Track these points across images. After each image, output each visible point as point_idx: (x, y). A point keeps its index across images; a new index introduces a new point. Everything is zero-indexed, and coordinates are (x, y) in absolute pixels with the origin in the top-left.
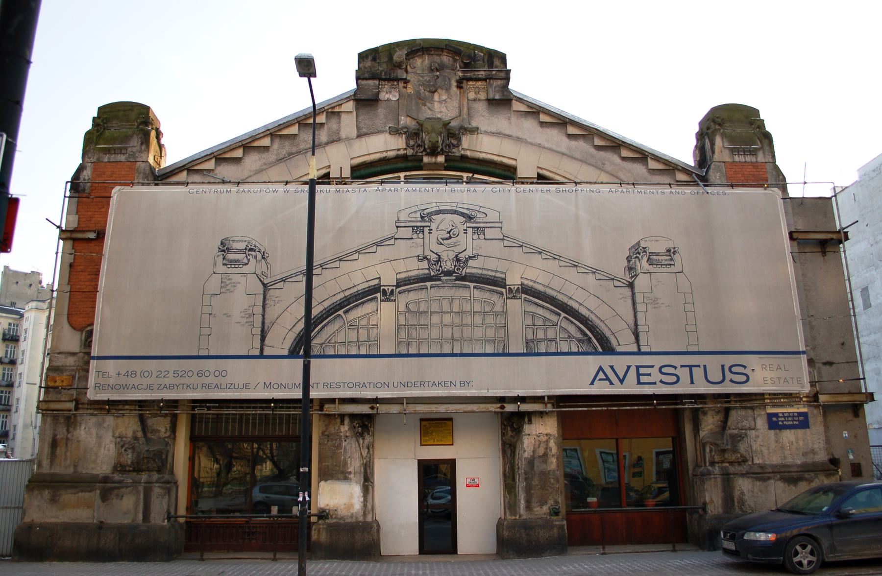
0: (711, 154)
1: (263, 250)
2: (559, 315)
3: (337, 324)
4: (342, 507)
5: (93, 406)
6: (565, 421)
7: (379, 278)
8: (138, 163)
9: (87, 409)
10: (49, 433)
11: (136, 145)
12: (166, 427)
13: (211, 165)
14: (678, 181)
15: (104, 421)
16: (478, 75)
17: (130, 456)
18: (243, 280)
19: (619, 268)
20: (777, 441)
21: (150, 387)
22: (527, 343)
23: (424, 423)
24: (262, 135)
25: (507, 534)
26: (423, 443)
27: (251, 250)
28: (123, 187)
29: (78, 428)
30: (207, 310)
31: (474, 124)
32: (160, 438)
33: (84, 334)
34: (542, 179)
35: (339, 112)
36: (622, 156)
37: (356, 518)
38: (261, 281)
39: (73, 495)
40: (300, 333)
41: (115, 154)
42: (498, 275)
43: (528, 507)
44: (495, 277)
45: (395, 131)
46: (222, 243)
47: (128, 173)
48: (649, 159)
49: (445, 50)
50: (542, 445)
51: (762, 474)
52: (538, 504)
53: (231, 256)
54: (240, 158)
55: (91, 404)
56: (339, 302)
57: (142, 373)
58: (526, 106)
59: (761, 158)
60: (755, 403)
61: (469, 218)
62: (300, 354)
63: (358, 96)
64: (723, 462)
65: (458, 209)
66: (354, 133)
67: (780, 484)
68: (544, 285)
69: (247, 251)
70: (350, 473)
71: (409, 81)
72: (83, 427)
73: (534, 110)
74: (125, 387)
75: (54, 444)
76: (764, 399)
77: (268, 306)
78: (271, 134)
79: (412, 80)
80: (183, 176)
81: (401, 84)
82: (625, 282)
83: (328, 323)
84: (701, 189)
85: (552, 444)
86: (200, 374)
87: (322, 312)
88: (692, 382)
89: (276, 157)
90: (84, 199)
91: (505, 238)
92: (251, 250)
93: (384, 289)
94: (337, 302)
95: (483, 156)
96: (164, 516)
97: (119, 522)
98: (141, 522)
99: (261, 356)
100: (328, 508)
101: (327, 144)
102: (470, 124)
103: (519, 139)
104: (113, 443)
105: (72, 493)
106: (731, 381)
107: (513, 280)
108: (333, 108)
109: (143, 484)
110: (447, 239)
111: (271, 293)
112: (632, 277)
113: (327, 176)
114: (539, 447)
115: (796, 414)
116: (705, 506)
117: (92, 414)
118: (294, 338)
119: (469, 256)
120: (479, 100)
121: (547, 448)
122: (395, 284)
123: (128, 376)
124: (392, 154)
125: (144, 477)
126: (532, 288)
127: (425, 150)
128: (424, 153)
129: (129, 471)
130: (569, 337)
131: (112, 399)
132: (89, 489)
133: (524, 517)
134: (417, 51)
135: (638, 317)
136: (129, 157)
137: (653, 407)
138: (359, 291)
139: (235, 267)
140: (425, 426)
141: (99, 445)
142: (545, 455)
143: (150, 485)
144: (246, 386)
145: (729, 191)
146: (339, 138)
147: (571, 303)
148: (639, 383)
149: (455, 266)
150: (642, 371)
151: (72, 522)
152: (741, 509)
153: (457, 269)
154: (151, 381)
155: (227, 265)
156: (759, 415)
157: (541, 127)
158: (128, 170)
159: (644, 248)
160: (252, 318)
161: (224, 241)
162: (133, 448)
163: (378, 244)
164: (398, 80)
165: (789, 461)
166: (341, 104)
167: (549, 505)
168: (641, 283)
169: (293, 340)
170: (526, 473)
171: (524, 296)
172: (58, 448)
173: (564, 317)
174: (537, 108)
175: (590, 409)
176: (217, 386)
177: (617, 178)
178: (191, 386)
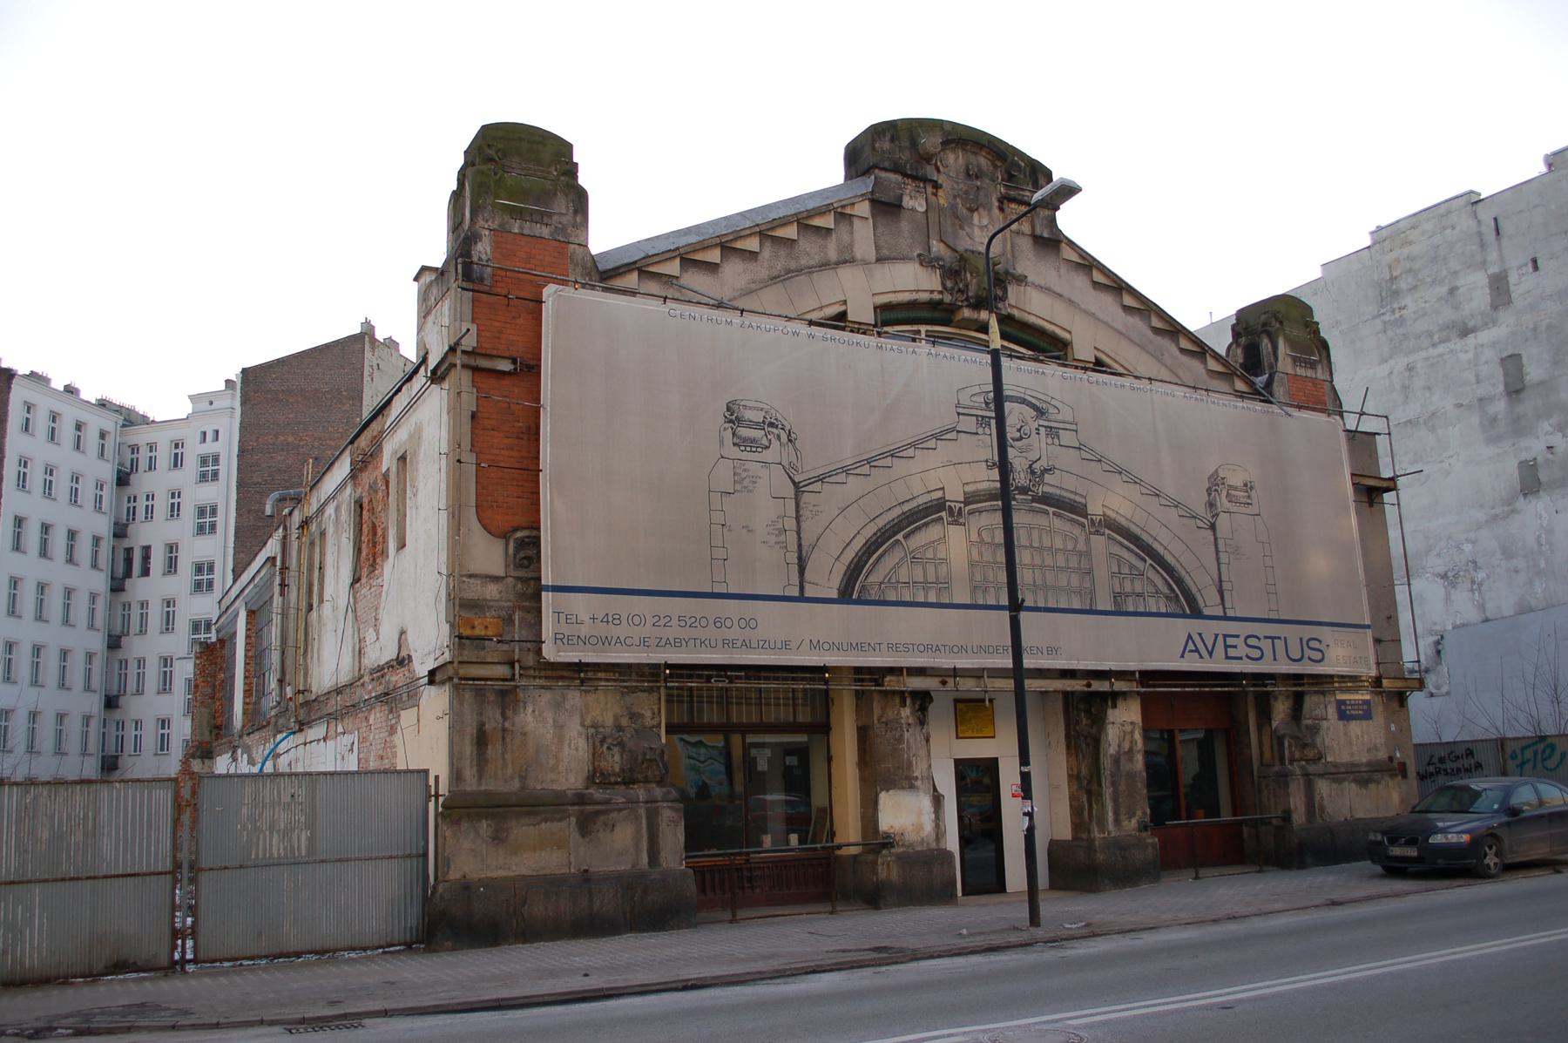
0: (1272, 360)
1: (788, 428)
2: (1145, 561)
3: (897, 555)
4: (910, 828)
5: (543, 673)
6: (1147, 702)
7: (943, 489)
8: (572, 246)
9: (535, 677)
10: (470, 719)
11: (564, 212)
12: (652, 709)
13: (673, 268)
14: (1237, 391)
15: (564, 697)
16: (1024, 196)
17: (617, 758)
18: (764, 473)
19: (1198, 503)
20: (1345, 734)
21: (644, 643)
22: (1115, 597)
23: (960, 706)
24: (748, 232)
25: (1102, 858)
26: (961, 735)
27: (771, 425)
28: (562, 287)
29: (522, 710)
30: (718, 518)
31: (1020, 270)
32: (645, 728)
33: (512, 544)
34: (1099, 365)
35: (851, 215)
36: (1182, 346)
37: (928, 844)
38: (790, 477)
39: (532, 827)
40: (850, 565)
41: (532, 221)
42: (1078, 499)
43: (1117, 822)
44: (1075, 501)
45: (927, 261)
46: (728, 409)
47: (555, 260)
48: (1208, 355)
49: (985, 149)
50: (1127, 737)
51: (1338, 774)
52: (1127, 816)
53: (744, 432)
54: (716, 264)
55: (540, 670)
56: (896, 521)
57: (630, 621)
58: (1077, 255)
59: (1320, 374)
60: (1326, 687)
61: (1040, 412)
62: (854, 597)
63: (877, 196)
64: (1301, 759)
65: (1026, 397)
66: (872, 255)
67: (1353, 786)
68: (1127, 519)
69: (766, 427)
70: (917, 778)
71: (941, 187)
72: (530, 709)
73: (1087, 263)
74: (606, 641)
75: (481, 740)
76: (1333, 683)
77: (803, 518)
78: (761, 233)
79: (944, 185)
80: (632, 280)
81: (930, 189)
82: (1206, 521)
83: (885, 551)
84: (1259, 406)
85: (1138, 736)
86: (718, 623)
87: (875, 534)
88: (1275, 659)
89: (767, 272)
90: (485, 296)
91: (1082, 447)
92: (771, 425)
93: (950, 506)
94: (893, 520)
95: (1032, 319)
96: (681, 855)
97: (612, 868)
98: (647, 867)
99: (802, 598)
100: (892, 831)
101: (838, 263)
102: (1014, 269)
103: (1071, 301)
104: (583, 736)
105: (529, 825)
106: (1309, 658)
107: (1095, 509)
108: (843, 207)
109: (642, 804)
110: (1018, 440)
111: (806, 498)
112: (1213, 516)
113: (842, 316)
114: (1124, 740)
115: (1360, 702)
116: (1290, 817)
117: (543, 687)
118: (842, 573)
119: (1045, 469)
120: (1023, 234)
121: (1132, 741)
122: (963, 500)
123: (608, 622)
124: (924, 297)
125: (640, 792)
126: (1115, 521)
127: (967, 299)
128: (966, 303)
129: (616, 783)
130: (1157, 593)
131: (587, 661)
132: (557, 816)
133: (1113, 835)
134: (953, 141)
135: (1222, 570)
136: (555, 232)
137: (1241, 689)
138: (920, 505)
139: (751, 451)
140: (961, 710)
141: (560, 739)
142: (1130, 752)
143: (654, 805)
144: (786, 645)
145: (1295, 412)
146: (853, 258)
147: (1156, 545)
148: (1227, 657)
149: (1030, 480)
150: (568, 617)
151: (535, 874)
152: (1321, 817)
153: (1033, 485)
154: (647, 631)
155: (740, 446)
156: (1330, 702)
157: (1094, 288)
158: (556, 254)
159: (1223, 479)
160: (784, 536)
161: (730, 405)
162: (621, 744)
163: (937, 437)
164: (925, 180)
165: (1356, 759)
166: (854, 204)
167: (1137, 818)
168: (1223, 522)
169: (841, 576)
170: (1112, 775)
171: (1107, 531)
172: (490, 747)
173: (1151, 565)
174: (1091, 260)
175: (1183, 689)
176: (744, 644)
177: (1178, 377)
178: (707, 642)
